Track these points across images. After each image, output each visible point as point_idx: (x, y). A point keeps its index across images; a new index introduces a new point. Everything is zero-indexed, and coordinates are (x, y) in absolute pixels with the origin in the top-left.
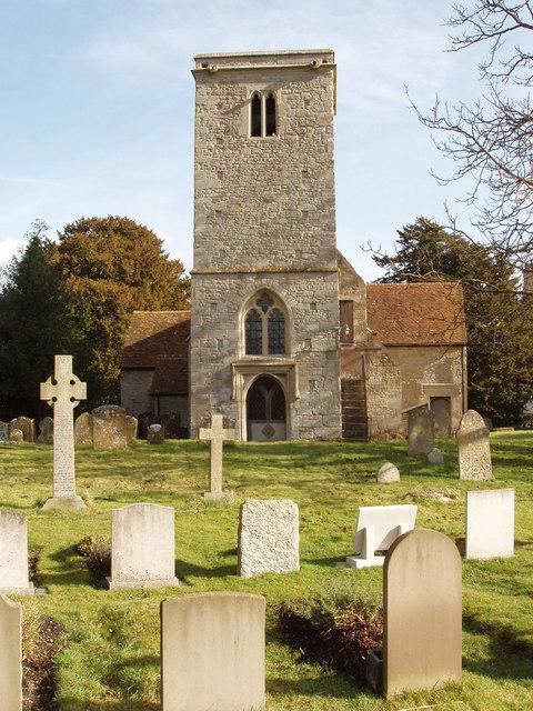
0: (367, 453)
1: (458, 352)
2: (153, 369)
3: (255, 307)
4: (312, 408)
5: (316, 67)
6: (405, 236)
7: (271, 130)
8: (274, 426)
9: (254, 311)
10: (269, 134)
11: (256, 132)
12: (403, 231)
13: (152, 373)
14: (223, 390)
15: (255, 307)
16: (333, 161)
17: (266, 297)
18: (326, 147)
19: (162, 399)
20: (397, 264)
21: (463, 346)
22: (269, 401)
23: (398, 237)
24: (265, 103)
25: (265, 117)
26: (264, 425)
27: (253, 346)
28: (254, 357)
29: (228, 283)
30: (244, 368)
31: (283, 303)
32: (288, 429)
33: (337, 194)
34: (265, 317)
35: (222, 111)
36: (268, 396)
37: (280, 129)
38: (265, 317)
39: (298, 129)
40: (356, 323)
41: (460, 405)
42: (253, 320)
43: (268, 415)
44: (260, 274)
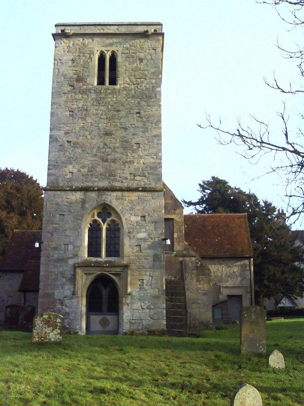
0: (131, 281)
1: (247, 262)
2: (23, 271)
3: (96, 218)
4: (141, 304)
5: (151, 34)
6: (203, 188)
7: (113, 81)
8: (109, 317)
9: (95, 221)
10: (110, 84)
11: (101, 81)
12: (202, 184)
13: (22, 275)
14: (66, 287)
15: (96, 218)
16: (160, 105)
17: (106, 210)
18: (155, 95)
19: (27, 294)
20: (198, 207)
21: (250, 258)
22: (105, 295)
23: (199, 188)
24: (110, 72)
25: (108, 69)
26: (102, 316)
27: (94, 249)
28: (93, 259)
29: (78, 195)
30: (85, 265)
31: (120, 218)
32: (121, 321)
33: (162, 113)
34: (104, 227)
35: (74, 64)
36: (105, 292)
37: (120, 81)
38: (104, 227)
39: (134, 80)
40: (175, 235)
41: (248, 301)
42: (94, 230)
43: (105, 306)
44: (101, 190)
